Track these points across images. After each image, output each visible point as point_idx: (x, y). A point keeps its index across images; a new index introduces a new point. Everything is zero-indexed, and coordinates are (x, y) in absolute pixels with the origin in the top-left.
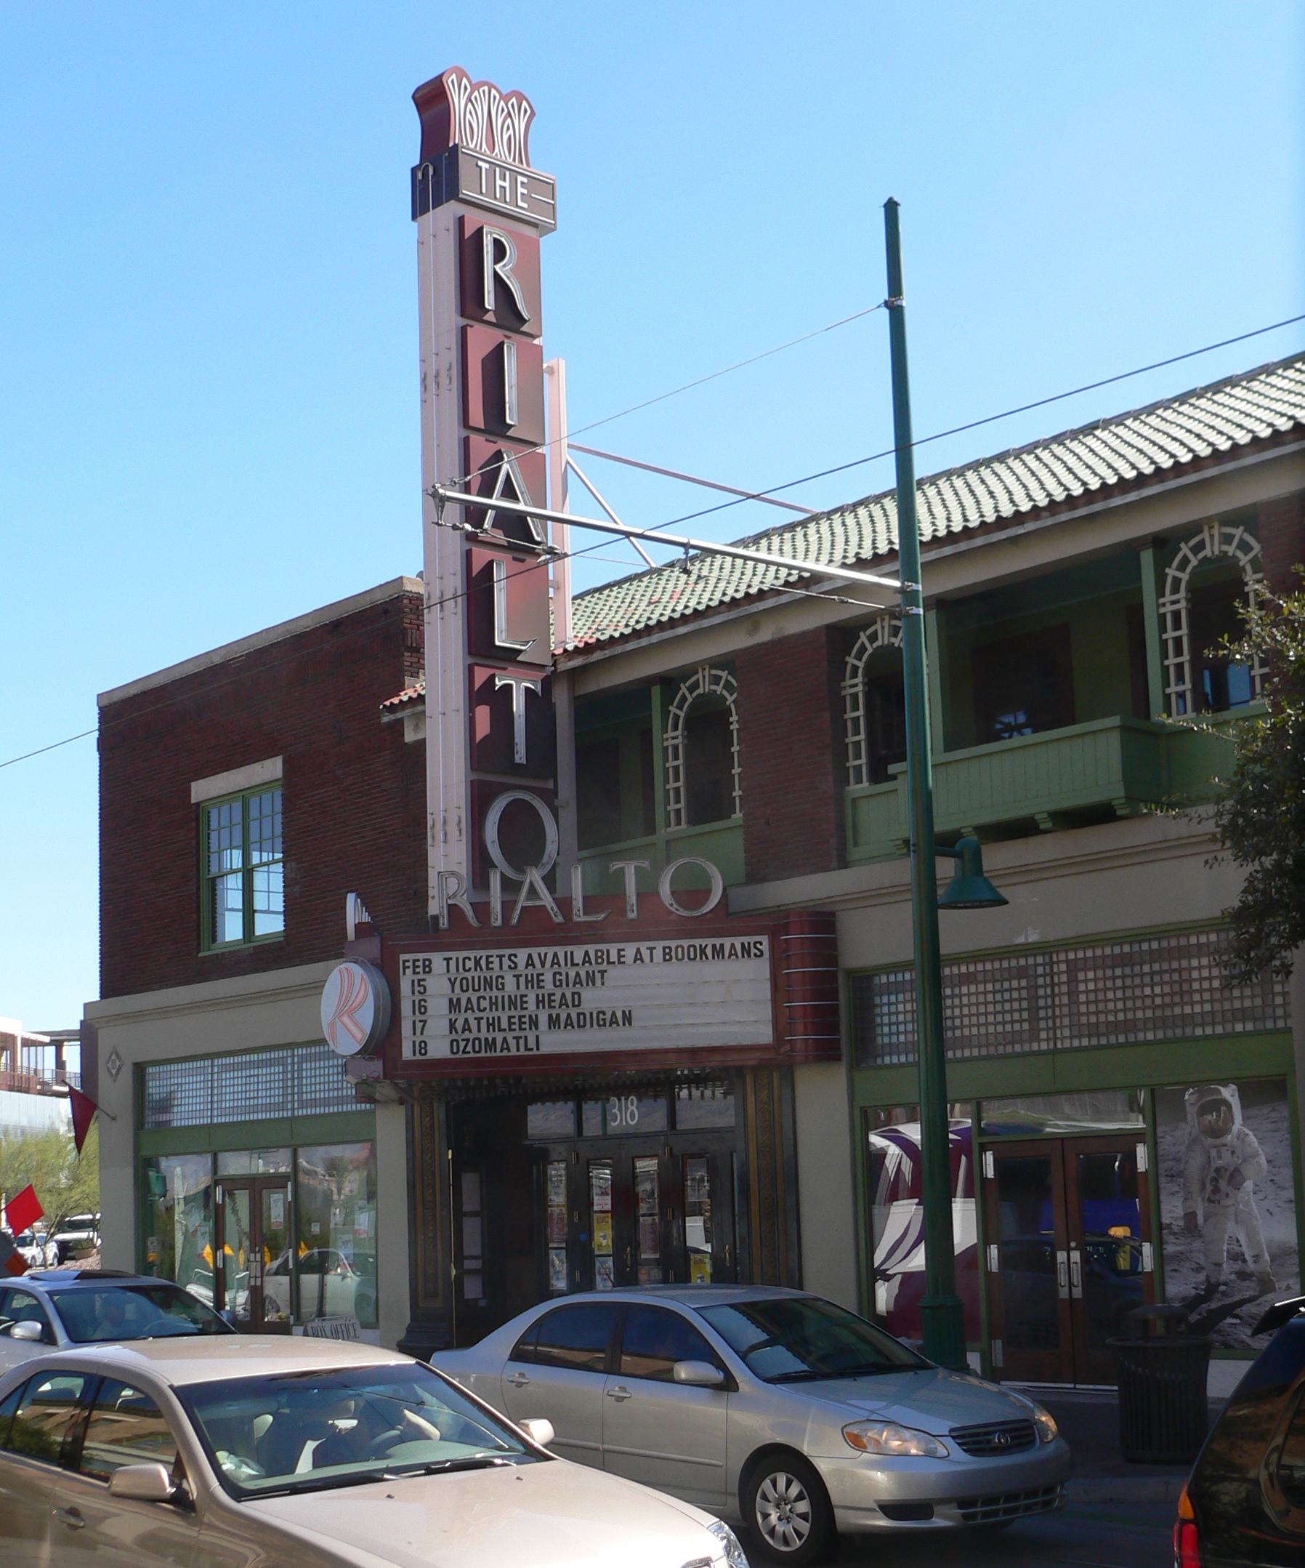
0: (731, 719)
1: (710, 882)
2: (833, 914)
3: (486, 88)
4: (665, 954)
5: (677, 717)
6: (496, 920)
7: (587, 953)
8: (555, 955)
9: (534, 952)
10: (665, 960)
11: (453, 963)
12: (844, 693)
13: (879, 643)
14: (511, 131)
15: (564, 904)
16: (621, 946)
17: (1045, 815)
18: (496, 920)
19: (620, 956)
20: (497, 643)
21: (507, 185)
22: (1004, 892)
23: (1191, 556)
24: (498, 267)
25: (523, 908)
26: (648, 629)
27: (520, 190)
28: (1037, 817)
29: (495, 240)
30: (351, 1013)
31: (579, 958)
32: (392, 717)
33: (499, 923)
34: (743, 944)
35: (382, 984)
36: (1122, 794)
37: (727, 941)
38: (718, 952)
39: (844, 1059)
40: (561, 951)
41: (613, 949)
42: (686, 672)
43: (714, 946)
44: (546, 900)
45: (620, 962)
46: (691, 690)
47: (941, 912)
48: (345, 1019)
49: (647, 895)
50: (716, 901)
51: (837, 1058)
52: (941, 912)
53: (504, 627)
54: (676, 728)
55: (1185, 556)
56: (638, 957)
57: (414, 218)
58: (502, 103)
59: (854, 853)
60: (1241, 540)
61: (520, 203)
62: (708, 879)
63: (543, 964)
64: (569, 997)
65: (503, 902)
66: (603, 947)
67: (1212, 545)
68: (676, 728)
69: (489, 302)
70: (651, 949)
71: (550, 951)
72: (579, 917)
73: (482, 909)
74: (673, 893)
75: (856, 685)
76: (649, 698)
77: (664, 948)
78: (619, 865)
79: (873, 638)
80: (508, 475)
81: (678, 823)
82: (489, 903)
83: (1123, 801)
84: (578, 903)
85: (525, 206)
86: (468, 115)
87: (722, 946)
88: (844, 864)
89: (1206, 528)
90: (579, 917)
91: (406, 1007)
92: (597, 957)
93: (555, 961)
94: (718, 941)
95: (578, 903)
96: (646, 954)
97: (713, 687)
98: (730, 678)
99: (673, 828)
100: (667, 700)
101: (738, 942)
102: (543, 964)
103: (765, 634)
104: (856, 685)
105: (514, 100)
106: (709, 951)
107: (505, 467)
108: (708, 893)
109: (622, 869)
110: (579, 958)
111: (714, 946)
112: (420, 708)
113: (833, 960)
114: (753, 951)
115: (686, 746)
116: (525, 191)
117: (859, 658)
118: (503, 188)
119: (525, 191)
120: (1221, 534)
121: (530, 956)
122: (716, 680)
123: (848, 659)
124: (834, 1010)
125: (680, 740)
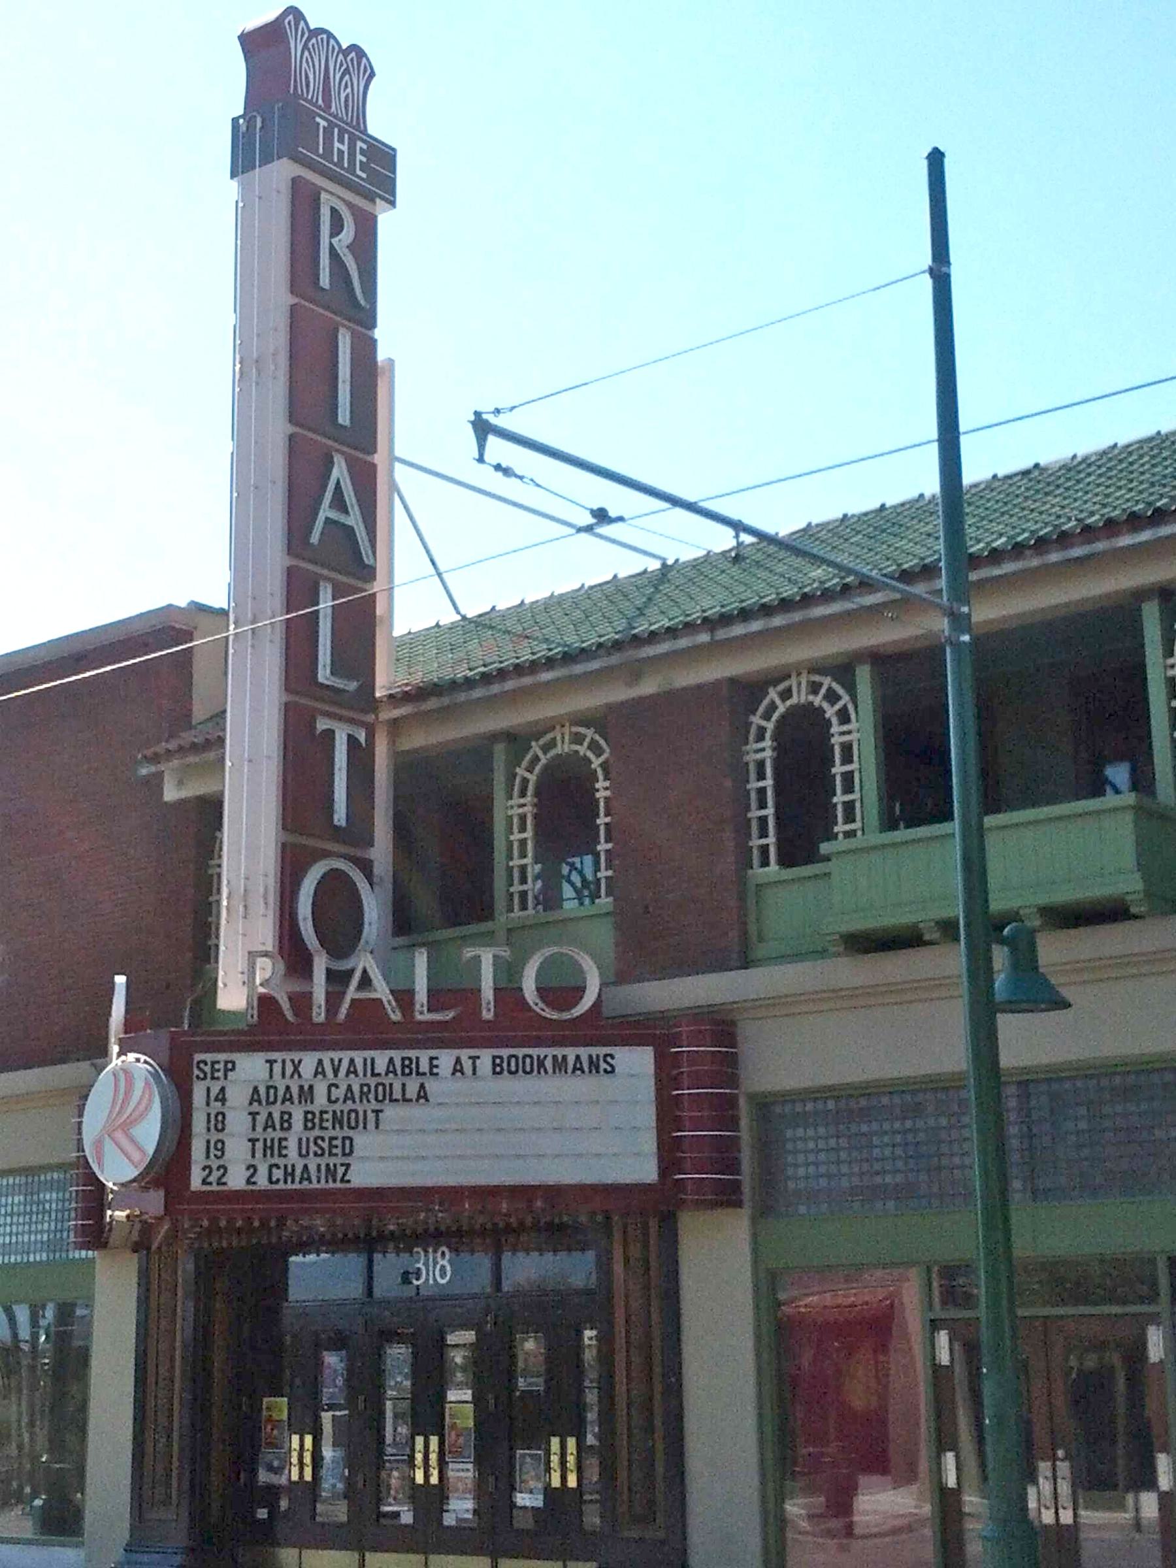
0: (597, 786)
1: (584, 980)
2: (733, 1023)
3: (325, 36)
4: (494, 1065)
5: (525, 781)
6: (319, 1015)
7: (391, 1060)
8: (352, 1061)
9: (327, 1056)
10: (494, 1073)
11: (277, 1068)
12: (747, 758)
13: (794, 700)
14: (349, 90)
15: (404, 997)
16: (433, 1053)
17: (933, 924)
18: (319, 1015)
19: (432, 1066)
20: (321, 679)
21: (345, 148)
22: (1067, 993)
23: (778, 701)
24: (335, 241)
25: (353, 1000)
26: (502, 674)
27: (359, 157)
28: (921, 925)
29: (332, 208)
30: (126, 1127)
31: (381, 1067)
32: (153, 769)
33: (322, 1018)
34: (590, 1057)
35: (171, 1091)
36: (1140, 886)
37: (571, 1053)
38: (560, 1065)
39: (747, 1204)
40: (359, 1056)
41: (424, 1056)
42: (538, 731)
43: (555, 1057)
44: (381, 990)
45: (432, 1074)
46: (546, 749)
47: (1002, 1019)
48: (119, 1135)
49: (509, 994)
50: (590, 1004)
51: (739, 1204)
52: (1002, 1019)
53: (328, 661)
54: (523, 794)
55: (773, 702)
56: (458, 1068)
57: (233, 175)
58: (341, 57)
59: (761, 951)
60: (830, 689)
61: (359, 172)
62: (580, 972)
63: (336, 1072)
64: (276, 1116)
65: (327, 993)
66: (412, 1054)
67: (799, 692)
68: (523, 794)
69: (325, 280)
70: (474, 1059)
71: (346, 1056)
72: (422, 1014)
73: (302, 1002)
74: (538, 989)
75: (763, 750)
76: (491, 755)
77: (494, 1058)
78: (469, 953)
79: (786, 695)
80: (338, 482)
81: (524, 907)
82: (311, 993)
83: (1142, 895)
84: (421, 997)
85: (364, 175)
86: (304, 65)
87: (564, 1057)
88: (746, 963)
89: (558, 727)
90: (422, 1014)
91: (199, 1123)
92: (403, 1066)
93: (352, 1070)
94: (559, 1052)
95: (421, 997)
96: (467, 1065)
97: (811, 698)
98: (597, 737)
99: (517, 913)
100: (515, 760)
101: (584, 1052)
102: (336, 1072)
103: (648, 687)
104: (763, 750)
105: (353, 54)
106: (548, 1063)
107: (335, 473)
108: (580, 990)
109: (477, 959)
110: (381, 1067)
111: (555, 1057)
112: (211, 755)
113: (733, 1080)
114: (603, 1066)
115: (535, 817)
116: (364, 159)
117: (530, 770)
118: (341, 152)
119: (364, 159)
120: (571, 732)
121: (320, 1062)
122: (578, 739)
123: (518, 770)
124: (734, 1142)
125: (528, 809)
